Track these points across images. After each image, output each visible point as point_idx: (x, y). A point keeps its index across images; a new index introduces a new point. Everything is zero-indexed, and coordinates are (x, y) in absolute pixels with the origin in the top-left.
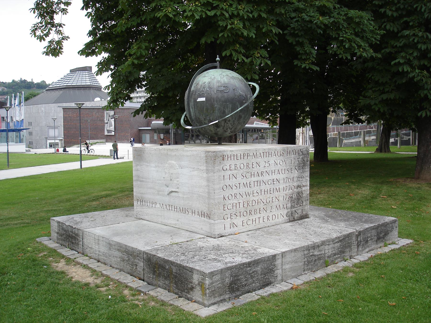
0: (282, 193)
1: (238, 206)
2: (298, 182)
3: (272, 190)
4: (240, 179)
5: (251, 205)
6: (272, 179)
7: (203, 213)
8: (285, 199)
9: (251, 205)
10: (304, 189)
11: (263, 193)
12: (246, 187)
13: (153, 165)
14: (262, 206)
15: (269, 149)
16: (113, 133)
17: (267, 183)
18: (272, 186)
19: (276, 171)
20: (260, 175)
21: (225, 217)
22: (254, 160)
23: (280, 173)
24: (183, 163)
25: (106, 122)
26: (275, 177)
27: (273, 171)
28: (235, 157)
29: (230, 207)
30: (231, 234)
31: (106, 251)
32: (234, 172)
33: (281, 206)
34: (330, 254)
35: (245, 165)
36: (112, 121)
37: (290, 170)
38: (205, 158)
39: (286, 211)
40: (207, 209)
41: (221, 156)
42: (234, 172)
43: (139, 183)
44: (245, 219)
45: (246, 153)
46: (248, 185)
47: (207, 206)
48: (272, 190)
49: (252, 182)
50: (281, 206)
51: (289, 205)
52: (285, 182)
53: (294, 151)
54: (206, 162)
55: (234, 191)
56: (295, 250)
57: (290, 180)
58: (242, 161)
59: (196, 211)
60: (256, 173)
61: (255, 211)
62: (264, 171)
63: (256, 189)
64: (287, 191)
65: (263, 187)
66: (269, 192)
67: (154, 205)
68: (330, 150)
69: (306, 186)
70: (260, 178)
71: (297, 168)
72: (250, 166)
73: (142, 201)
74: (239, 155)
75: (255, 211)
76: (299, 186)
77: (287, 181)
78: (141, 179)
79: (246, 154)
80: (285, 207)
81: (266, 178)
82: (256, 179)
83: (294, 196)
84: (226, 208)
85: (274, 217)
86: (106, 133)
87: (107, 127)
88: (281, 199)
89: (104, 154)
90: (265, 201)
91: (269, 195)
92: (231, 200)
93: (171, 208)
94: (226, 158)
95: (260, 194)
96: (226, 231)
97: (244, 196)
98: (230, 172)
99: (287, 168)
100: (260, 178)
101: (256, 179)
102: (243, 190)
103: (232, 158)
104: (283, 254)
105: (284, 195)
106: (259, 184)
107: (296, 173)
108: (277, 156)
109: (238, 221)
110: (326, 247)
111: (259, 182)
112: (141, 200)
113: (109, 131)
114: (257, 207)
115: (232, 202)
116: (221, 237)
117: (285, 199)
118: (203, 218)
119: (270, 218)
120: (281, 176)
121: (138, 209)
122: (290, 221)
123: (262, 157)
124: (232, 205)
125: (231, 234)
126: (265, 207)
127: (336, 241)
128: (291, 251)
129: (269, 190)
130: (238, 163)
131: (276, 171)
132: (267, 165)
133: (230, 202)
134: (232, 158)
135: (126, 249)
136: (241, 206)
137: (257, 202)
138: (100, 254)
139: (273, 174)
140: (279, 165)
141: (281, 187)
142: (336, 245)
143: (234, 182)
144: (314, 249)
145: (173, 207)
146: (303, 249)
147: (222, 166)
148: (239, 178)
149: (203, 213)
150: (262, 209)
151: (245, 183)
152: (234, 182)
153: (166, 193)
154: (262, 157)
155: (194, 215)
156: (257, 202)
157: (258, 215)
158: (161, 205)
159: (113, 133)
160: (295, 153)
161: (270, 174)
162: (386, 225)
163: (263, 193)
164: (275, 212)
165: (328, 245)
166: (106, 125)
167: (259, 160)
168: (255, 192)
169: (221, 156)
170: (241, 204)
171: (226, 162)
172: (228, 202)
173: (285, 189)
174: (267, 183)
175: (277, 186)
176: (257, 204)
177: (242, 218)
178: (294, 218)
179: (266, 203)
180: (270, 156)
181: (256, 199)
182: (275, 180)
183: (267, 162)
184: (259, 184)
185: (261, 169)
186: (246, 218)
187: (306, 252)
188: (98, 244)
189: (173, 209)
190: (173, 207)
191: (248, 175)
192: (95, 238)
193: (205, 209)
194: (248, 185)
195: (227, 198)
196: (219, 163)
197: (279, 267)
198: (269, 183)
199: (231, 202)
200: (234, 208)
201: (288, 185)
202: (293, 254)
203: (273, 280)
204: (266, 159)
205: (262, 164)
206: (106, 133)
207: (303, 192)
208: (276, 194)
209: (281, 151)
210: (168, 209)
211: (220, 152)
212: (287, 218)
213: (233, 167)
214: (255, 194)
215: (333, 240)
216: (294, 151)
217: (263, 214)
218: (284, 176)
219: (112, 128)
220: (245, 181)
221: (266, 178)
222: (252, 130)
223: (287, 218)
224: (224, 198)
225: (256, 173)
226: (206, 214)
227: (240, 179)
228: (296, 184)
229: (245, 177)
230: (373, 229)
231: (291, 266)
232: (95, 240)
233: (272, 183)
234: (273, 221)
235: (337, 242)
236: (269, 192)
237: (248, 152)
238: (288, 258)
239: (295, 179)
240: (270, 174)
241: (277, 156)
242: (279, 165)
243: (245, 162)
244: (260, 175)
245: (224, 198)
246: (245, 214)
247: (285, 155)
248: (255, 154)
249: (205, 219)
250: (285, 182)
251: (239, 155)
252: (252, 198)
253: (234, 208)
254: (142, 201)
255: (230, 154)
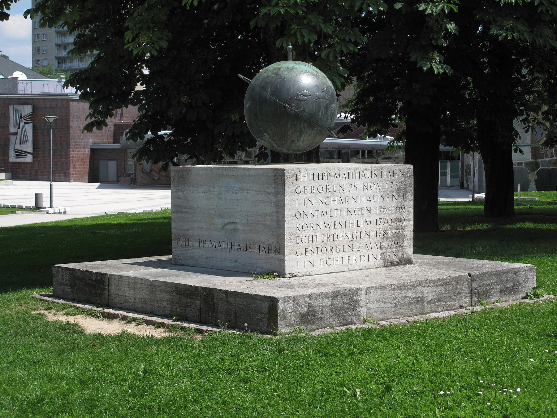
0: (374, 228)
1: (315, 239)
2: (397, 214)
3: (360, 222)
4: (317, 206)
5: (331, 239)
6: (360, 207)
7: (270, 248)
8: (378, 236)
9: (331, 239)
10: (405, 223)
11: (348, 225)
12: (326, 215)
13: (201, 190)
14: (346, 241)
15: (356, 168)
16: (29, 159)
17: (353, 213)
18: (360, 217)
19: (366, 198)
20: (344, 202)
21: (299, 253)
22: (336, 182)
23: (372, 200)
24: (244, 185)
25: (12, 130)
26: (364, 205)
27: (362, 198)
28: (312, 176)
29: (305, 240)
30: (306, 275)
31: (145, 296)
32: (310, 196)
33: (373, 245)
34: (429, 299)
35: (325, 187)
36: (29, 128)
37: (385, 197)
38: (273, 178)
39: (379, 252)
40: (275, 242)
41: (294, 175)
42: (310, 196)
43: (180, 215)
44: (324, 257)
45: (325, 172)
46: (328, 213)
47: (276, 238)
48: (360, 222)
49: (333, 210)
50: (373, 245)
51: (385, 244)
52: (378, 212)
53: (391, 172)
54: (275, 182)
55: (309, 221)
56: (384, 288)
57: (385, 210)
58: (320, 182)
59: (262, 246)
60: (338, 198)
61: (338, 248)
62: (350, 196)
63: (339, 219)
64: (382, 225)
65: (348, 217)
66: (356, 225)
67: (202, 245)
68: (518, 196)
69: (409, 220)
70: (345, 206)
71: (395, 194)
72: (331, 189)
73: (184, 239)
74: (316, 174)
75: (338, 248)
76: (398, 220)
77: (382, 211)
78: (184, 210)
79: (326, 174)
80: (378, 246)
81: (352, 205)
82: (339, 206)
83: (392, 233)
84: (299, 241)
85: (363, 257)
86: (13, 158)
87: (15, 144)
88: (373, 235)
89: (24, 205)
90: (351, 236)
91: (355, 229)
92: (307, 231)
93: (226, 246)
94: (300, 177)
95: (343, 226)
96: (299, 270)
97: (323, 228)
98: (305, 196)
99: (382, 194)
100: (345, 206)
101: (339, 206)
102: (321, 220)
103: (308, 177)
104: (368, 290)
105: (378, 230)
106: (342, 213)
107: (393, 202)
108: (367, 177)
109: (315, 258)
110: (425, 289)
111: (342, 211)
112: (184, 238)
113: (20, 153)
114: (339, 242)
115: (308, 234)
116: (293, 276)
117: (378, 236)
118: (270, 254)
119: (358, 259)
120: (372, 205)
121: (178, 252)
122: (385, 266)
123: (347, 178)
124: (307, 237)
125: (306, 275)
126: (350, 244)
127: (439, 283)
128: (378, 288)
129: (356, 223)
130: (316, 184)
131: (366, 198)
132: (353, 188)
133: (305, 233)
134: (308, 177)
135: (176, 288)
136: (319, 240)
137: (339, 236)
138: (137, 301)
139: (362, 201)
140: (369, 189)
141: (373, 219)
142: (439, 288)
143: (310, 208)
144: (408, 289)
145: (230, 244)
146: (393, 287)
147: (294, 188)
148: (317, 204)
149: (270, 248)
150: (346, 246)
151: (324, 211)
152: (310, 208)
153: (220, 227)
154: (347, 178)
155: (258, 251)
156: (339, 236)
157: (341, 254)
158: (213, 243)
159: (29, 159)
160: (392, 175)
161: (358, 200)
162: (516, 272)
163: (348, 225)
164: (364, 251)
165: (428, 287)
166: (12, 138)
167: (342, 182)
168: (337, 223)
169: (294, 175)
170: (319, 238)
171: (299, 182)
172: (302, 233)
173: (378, 222)
174: (353, 213)
175: (366, 217)
176: (339, 239)
177: (320, 256)
178: (391, 263)
179: (352, 239)
180: (358, 177)
181: (338, 232)
182: (364, 209)
183: (353, 184)
184: (342, 213)
185: (346, 194)
186: (325, 256)
187: (397, 292)
188: (134, 289)
189: (230, 247)
190: (230, 244)
191: (328, 201)
192: (129, 282)
193: (273, 243)
194: (328, 213)
195: (301, 229)
196: (291, 183)
197: (363, 304)
198: (357, 213)
199: (306, 233)
200: (310, 242)
201: (382, 217)
202: (380, 292)
203: (354, 319)
204: (352, 181)
205: (347, 187)
206: (13, 158)
207: (405, 228)
208: (366, 228)
209: (373, 171)
210: (223, 247)
211: (292, 170)
212: (382, 262)
213: (308, 190)
214: (338, 226)
215: (434, 282)
216: (391, 172)
217: (348, 253)
218: (377, 204)
219: (28, 147)
220: (323, 208)
221: (352, 205)
222: (363, 153)
223: (382, 262)
224: (297, 228)
225: (338, 198)
226: (274, 249)
227: (317, 206)
228: (393, 216)
229: (324, 203)
230: (495, 275)
231: (377, 305)
232: (129, 285)
233: (360, 213)
234: (362, 264)
235: (440, 285)
236: (356, 225)
237: (329, 171)
238: (375, 295)
239: (393, 210)
240: (358, 200)
241: (367, 177)
242: (369, 189)
243: (324, 183)
244: (344, 202)
245: (297, 228)
246: (324, 251)
247: (379, 176)
248: (337, 174)
249: (273, 255)
250: (378, 212)
251: (316, 174)
252: (333, 231)
253: (310, 242)
254: (184, 239)
255: (305, 173)
